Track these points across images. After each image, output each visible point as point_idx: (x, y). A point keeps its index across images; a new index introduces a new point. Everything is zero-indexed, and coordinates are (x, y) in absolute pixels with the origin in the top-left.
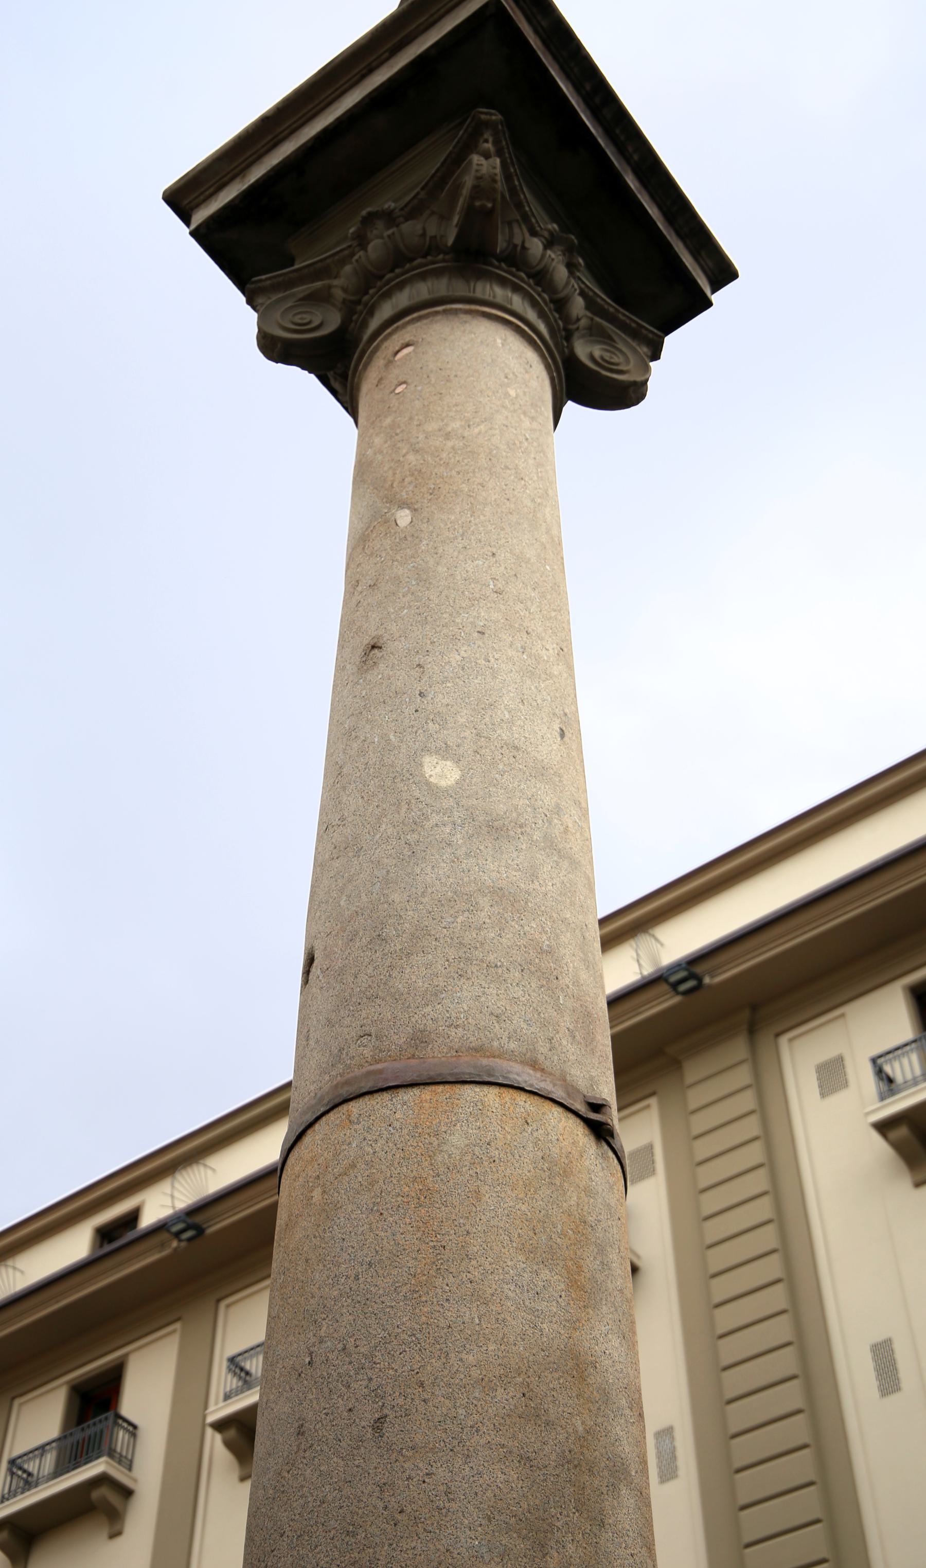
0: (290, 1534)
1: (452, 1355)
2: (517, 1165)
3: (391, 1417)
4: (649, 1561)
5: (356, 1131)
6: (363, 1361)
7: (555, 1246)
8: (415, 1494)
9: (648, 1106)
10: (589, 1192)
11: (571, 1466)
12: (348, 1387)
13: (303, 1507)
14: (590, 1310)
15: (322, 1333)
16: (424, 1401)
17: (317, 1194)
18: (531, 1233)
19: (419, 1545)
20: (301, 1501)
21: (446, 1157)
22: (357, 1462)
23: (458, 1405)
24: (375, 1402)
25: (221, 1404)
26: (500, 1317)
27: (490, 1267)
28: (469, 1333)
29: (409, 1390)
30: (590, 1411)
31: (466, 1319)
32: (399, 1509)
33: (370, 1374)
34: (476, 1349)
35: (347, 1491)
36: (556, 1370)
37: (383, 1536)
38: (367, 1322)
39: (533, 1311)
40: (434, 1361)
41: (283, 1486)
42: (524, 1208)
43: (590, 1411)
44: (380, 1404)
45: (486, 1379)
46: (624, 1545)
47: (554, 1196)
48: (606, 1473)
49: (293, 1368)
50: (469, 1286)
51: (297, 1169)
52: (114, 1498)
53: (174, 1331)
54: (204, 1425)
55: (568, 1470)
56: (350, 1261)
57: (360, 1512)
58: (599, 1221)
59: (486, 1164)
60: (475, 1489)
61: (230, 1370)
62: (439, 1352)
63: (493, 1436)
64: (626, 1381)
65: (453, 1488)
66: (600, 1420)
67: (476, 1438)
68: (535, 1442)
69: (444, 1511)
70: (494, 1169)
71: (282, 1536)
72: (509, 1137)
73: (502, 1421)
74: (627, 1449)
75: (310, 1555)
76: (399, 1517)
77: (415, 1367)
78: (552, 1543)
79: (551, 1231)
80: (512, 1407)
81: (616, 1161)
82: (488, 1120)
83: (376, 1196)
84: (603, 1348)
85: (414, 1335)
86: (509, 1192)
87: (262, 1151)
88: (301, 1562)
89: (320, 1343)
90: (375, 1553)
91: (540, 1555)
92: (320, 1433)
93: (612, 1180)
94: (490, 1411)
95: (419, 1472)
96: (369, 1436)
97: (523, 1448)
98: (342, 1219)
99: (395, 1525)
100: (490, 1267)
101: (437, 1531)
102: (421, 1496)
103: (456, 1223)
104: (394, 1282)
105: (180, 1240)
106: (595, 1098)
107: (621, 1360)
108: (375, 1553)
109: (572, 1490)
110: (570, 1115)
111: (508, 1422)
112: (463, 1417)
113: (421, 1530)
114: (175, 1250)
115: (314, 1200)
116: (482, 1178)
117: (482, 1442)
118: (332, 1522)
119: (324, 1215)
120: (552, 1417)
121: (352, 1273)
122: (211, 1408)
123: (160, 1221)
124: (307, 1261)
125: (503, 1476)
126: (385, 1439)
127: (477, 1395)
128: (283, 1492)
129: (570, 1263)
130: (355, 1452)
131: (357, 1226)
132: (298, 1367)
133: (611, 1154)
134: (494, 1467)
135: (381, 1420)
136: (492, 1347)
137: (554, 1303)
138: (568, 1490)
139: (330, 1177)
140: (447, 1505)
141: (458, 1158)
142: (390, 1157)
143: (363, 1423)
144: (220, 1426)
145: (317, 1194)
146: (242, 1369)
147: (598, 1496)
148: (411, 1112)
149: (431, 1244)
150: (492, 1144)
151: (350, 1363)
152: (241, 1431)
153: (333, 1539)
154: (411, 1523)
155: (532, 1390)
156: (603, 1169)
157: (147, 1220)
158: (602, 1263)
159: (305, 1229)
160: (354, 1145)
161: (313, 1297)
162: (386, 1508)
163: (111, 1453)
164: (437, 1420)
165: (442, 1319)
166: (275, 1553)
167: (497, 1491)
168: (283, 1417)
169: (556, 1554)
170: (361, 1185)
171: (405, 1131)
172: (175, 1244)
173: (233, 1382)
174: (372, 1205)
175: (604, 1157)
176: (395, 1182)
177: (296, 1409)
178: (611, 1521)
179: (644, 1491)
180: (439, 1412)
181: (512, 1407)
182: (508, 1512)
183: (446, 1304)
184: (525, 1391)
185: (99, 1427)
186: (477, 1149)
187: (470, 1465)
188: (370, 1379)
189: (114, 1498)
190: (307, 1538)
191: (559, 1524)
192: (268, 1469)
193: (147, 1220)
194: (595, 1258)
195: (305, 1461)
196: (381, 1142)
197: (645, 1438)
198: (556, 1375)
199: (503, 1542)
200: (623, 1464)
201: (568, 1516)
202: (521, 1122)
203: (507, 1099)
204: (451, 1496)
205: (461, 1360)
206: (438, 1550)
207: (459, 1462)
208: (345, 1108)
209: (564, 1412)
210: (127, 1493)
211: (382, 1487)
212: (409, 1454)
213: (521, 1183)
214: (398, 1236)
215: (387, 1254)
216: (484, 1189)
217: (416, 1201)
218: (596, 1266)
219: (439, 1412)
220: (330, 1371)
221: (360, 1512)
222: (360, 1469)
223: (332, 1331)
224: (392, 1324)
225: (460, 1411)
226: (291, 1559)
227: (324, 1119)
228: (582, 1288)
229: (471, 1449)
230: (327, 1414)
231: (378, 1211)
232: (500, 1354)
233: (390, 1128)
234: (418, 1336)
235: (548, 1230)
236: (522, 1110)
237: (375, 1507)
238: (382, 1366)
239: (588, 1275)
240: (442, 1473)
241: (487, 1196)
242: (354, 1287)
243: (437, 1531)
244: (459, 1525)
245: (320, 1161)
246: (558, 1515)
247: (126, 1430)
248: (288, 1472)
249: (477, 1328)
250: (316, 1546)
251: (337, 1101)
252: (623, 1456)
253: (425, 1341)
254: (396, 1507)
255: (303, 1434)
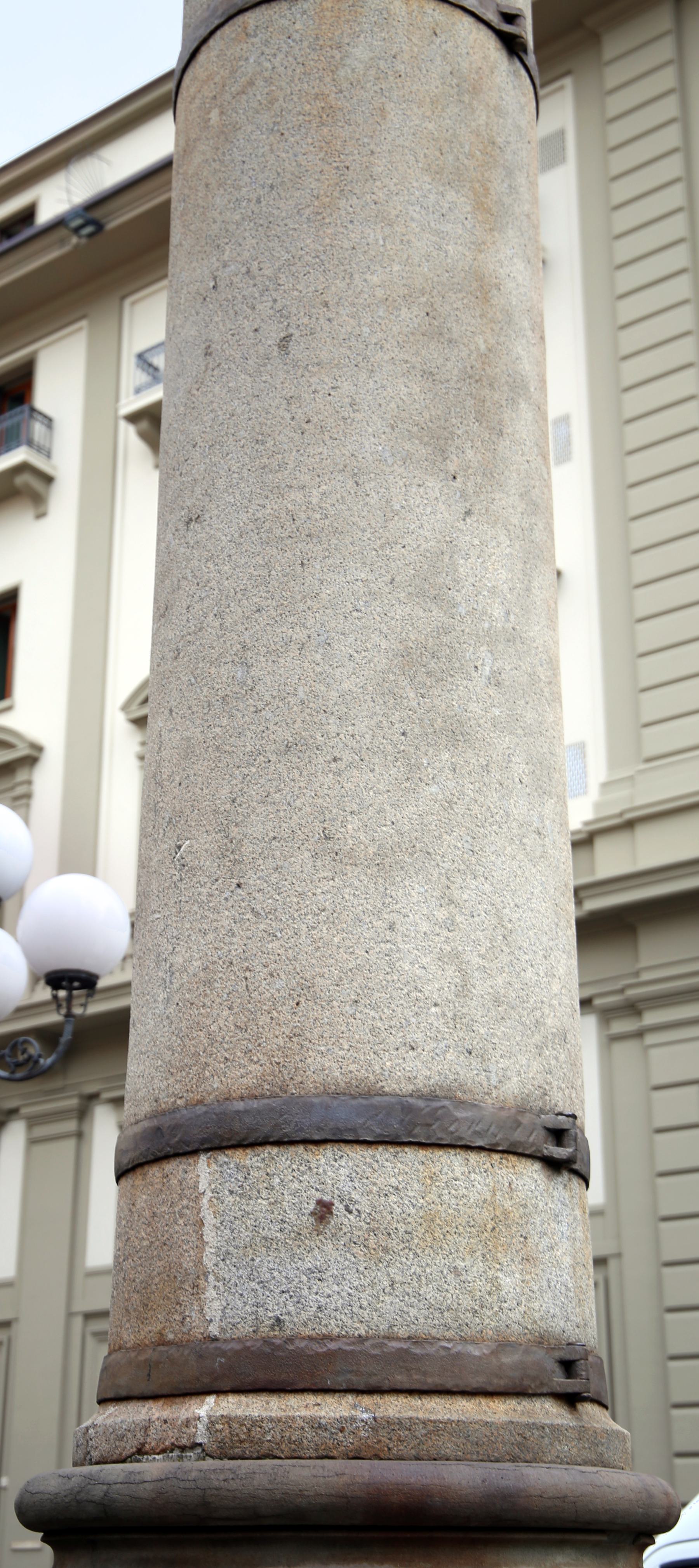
0: (202, 444)
1: (356, 276)
2: (424, 80)
3: (297, 335)
4: (543, 468)
5: (253, 44)
6: (267, 283)
7: (462, 167)
8: (321, 406)
9: (562, 88)
10: (499, 111)
11: (472, 381)
12: (253, 308)
13: (213, 420)
14: (496, 234)
15: (226, 257)
16: (329, 320)
17: (214, 115)
18: (438, 153)
19: (325, 451)
20: (212, 415)
21: (349, 71)
22: (264, 379)
23: (362, 323)
24: (280, 322)
25: (132, 398)
26: (405, 238)
27: (394, 188)
28: (374, 254)
29: (313, 310)
30: (492, 330)
31: (370, 240)
32: (306, 420)
33: (274, 296)
34: (380, 270)
35: (255, 404)
36: (460, 291)
37: (291, 444)
38: (270, 244)
39: (437, 233)
40: (338, 281)
41: (193, 403)
42: (430, 126)
43: (492, 330)
44: (286, 324)
45: (390, 299)
46: (520, 452)
47: (462, 114)
48: (506, 388)
49: (199, 293)
50: (373, 207)
51: (192, 90)
52: (37, 484)
53: (80, 329)
54: (116, 418)
55: (470, 384)
56: (251, 183)
57: (269, 422)
58: (508, 143)
59: (391, 79)
60: (379, 401)
61: (138, 366)
62: (343, 274)
63: (397, 353)
64: (529, 304)
65: (358, 400)
66: (502, 339)
67: (380, 354)
68: (437, 358)
69: (349, 421)
70: (400, 85)
71: (194, 446)
72: (416, 49)
73: (406, 339)
74: (527, 367)
75: (222, 462)
76: (306, 426)
77: (320, 287)
78: (453, 449)
79: (458, 151)
80: (416, 326)
81: (528, 80)
82: (393, 30)
83: (276, 116)
84: (508, 271)
85: (318, 257)
86: (416, 110)
87: (154, 142)
88: (214, 468)
89: (224, 266)
90: (283, 458)
91: (440, 459)
92: (227, 352)
93: (523, 100)
94: (394, 329)
95: (325, 386)
96: (275, 354)
97: (426, 364)
98: (242, 141)
99: (302, 433)
100: (394, 188)
101: (343, 439)
102: (327, 408)
103: (360, 143)
104: (297, 205)
105: (80, 237)
106: (508, 7)
107: (525, 283)
108: (283, 458)
109: (472, 402)
110: (482, 27)
111: (412, 339)
112: (367, 335)
113: (327, 438)
114: (77, 247)
115: (212, 122)
116: (387, 94)
117: (386, 358)
118: (242, 433)
119: (222, 137)
120: (455, 336)
121: (254, 197)
122: (123, 401)
123: (57, 217)
124: (207, 185)
125: (406, 389)
126: (291, 356)
127: (381, 314)
128: (193, 408)
129: (477, 185)
130: (262, 369)
131: (258, 147)
132: (202, 291)
133: (523, 72)
134: (397, 380)
135: (287, 338)
136: (396, 268)
137: (460, 225)
138: (470, 402)
139: (228, 97)
140: (352, 415)
141: (362, 72)
142: (290, 73)
143: (269, 342)
144: (133, 418)
145: (214, 115)
146: (150, 365)
147: (498, 408)
148: (311, 22)
149: (335, 164)
150: (398, 57)
151: (255, 285)
152: (149, 420)
153: (243, 447)
154: (318, 431)
155: (436, 310)
156: (514, 88)
157: (44, 216)
158: (510, 186)
159: (204, 153)
160: (252, 61)
161: (215, 222)
162: (293, 418)
163: (30, 443)
164: (341, 337)
165: (346, 241)
166: (189, 462)
167: (400, 403)
168: (190, 339)
169: (455, 459)
170: (261, 104)
171: (305, 44)
172: (74, 240)
173: (143, 378)
174: (271, 125)
175: (516, 73)
176: (296, 99)
177: (203, 332)
178: (509, 431)
179: (542, 407)
180: (343, 331)
181: (416, 326)
182: (411, 421)
183: (350, 226)
184: (429, 310)
185: (15, 420)
186: (382, 63)
187: (375, 379)
188: (275, 301)
189: (37, 484)
190: (218, 447)
191: (459, 432)
192: (178, 388)
193: (44, 216)
194: (503, 181)
195: (213, 379)
196: (280, 56)
197: (545, 359)
198: (460, 296)
199: (406, 448)
200: (523, 381)
201: (469, 425)
202: (429, 32)
203: (414, 7)
204: (356, 407)
205: (365, 280)
206: (344, 455)
207: (363, 376)
208: (240, 19)
209: (466, 330)
210: (49, 480)
211: (289, 400)
212: (315, 369)
213: (428, 100)
214: (300, 158)
215: (289, 176)
216: (389, 106)
217: (318, 119)
218: (503, 190)
219: (343, 331)
220: (234, 294)
221: (269, 422)
222: (267, 384)
223: (235, 255)
224: (296, 247)
225: (366, 329)
226: (204, 466)
227: (219, 33)
228: (488, 211)
229: (375, 364)
230: (233, 335)
231: (278, 131)
232: (404, 274)
233: (290, 41)
234: (322, 257)
235: (455, 150)
236: (431, 19)
237: (282, 418)
238: (287, 288)
239: (495, 198)
240: (346, 387)
241: (392, 113)
242: (257, 211)
243: (343, 439)
244: (363, 433)
245: (216, 80)
246: (459, 425)
247: (42, 423)
248: (198, 390)
249: (382, 249)
250: (228, 454)
251: (232, 11)
252: (523, 373)
253: (329, 262)
254: (303, 417)
255: (210, 354)
